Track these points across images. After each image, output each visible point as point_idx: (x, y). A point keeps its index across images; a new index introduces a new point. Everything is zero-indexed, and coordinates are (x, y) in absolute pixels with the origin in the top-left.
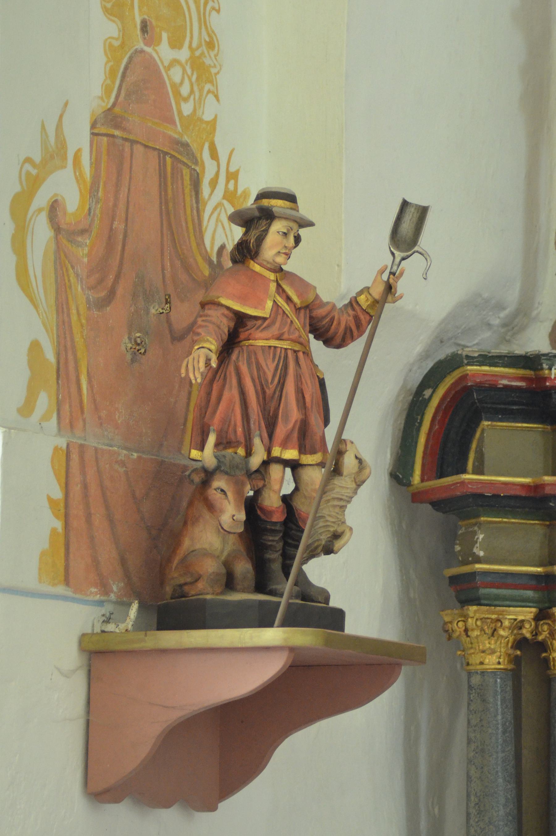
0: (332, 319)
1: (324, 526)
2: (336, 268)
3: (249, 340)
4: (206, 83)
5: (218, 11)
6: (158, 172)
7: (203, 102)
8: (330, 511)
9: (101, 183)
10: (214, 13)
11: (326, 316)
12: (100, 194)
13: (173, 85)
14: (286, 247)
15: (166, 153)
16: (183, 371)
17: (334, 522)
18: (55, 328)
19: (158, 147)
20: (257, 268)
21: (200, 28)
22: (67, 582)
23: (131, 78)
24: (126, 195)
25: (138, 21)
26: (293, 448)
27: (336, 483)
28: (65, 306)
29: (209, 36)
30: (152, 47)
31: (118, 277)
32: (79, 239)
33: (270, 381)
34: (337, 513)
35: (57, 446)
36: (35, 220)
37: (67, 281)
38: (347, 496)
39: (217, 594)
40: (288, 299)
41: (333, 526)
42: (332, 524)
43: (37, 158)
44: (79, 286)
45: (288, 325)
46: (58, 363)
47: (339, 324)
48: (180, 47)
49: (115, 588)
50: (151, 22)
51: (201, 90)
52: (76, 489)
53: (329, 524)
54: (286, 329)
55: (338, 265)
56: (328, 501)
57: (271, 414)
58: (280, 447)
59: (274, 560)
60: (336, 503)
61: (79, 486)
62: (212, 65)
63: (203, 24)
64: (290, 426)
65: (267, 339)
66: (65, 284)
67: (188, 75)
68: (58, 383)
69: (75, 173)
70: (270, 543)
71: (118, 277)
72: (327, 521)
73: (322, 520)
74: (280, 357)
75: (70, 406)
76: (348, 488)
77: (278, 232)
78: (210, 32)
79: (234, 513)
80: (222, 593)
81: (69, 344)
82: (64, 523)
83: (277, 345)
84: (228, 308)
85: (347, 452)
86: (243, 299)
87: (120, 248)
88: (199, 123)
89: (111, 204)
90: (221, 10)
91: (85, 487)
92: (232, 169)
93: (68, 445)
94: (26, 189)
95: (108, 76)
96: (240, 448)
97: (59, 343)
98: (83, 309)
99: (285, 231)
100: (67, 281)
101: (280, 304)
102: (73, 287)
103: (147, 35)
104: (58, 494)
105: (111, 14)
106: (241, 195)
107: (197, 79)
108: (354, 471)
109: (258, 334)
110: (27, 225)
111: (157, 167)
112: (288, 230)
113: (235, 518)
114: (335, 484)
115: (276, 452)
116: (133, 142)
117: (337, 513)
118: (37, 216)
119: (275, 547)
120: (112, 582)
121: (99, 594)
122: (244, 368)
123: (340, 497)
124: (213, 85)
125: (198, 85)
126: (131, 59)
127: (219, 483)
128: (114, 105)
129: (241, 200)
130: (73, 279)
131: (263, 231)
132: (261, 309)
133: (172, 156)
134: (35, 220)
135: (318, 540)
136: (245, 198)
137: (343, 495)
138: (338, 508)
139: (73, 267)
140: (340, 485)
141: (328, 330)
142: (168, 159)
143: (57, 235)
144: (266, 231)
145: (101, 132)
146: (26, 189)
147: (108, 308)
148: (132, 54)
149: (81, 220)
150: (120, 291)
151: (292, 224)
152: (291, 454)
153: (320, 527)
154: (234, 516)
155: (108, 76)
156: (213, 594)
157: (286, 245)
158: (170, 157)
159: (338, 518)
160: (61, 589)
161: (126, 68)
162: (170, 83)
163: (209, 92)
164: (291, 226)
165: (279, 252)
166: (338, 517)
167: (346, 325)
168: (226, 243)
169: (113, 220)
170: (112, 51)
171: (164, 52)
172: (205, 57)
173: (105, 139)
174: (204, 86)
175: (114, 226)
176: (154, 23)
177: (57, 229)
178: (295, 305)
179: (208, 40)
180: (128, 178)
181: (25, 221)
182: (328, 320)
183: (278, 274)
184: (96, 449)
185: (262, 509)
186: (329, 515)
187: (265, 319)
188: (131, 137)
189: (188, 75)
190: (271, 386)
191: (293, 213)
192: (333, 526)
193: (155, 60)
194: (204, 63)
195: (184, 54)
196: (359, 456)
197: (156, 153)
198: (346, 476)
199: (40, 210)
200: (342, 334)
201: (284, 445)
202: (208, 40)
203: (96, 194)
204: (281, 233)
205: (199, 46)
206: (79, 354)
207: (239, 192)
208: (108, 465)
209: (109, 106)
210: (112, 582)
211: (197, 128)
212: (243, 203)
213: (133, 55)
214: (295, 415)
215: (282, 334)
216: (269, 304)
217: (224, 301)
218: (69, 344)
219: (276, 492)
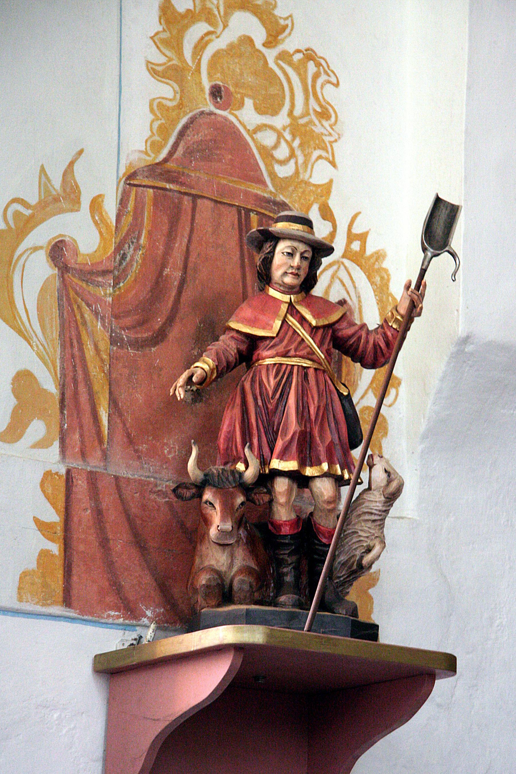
0: (360, 338)
1: (357, 542)
2: (456, 312)
3: (259, 360)
4: (315, 149)
5: (337, 85)
6: (236, 226)
7: (310, 167)
8: (362, 526)
9: (144, 232)
10: (329, 88)
11: (353, 335)
12: (142, 241)
13: (262, 149)
14: (292, 267)
15: (248, 211)
16: (172, 391)
17: (367, 537)
18: (58, 361)
19: (237, 204)
20: (272, 292)
21: (307, 99)
22: (67, 601)
23: (192, 137)
24: (184, 244)
25: (207, 85)
26: (293, 459)
27: (365, 497)
28: (75, 342)
29: (321, 106)
30: (229, 110)
31: (170, 320)
32: (100, 279)
33: (270, 396)
34: (369, 528)
35: (51, 471)
36: (28, 256)
37: (78, 317)
38: (376, 510)
39: (213, 607)
40: (302, 320)
41: (366, 541)
42: (366, 539)
43: (33, 199)
44: (99, 324)
45: (296, 343)
46: (63, 394)
47: (367, 341)
48: (275, 112)
49: (149, 613)
50: (227, 89)
51: (307, 156)
52: (84, 514)
53: (362, 539)
54: (293, 347)
55: (457, 310)
56: (359, 516)
57: (275, 429)
58: (277, 459)
59: (287, 574)
60: (367, 517)
61: (89, 511)
62: (325, 132)
63: (311, 94)
64: (289, 437)
65: (272, 357)
66: (76, 321)
67: (286, 141)
68: (62, 413)
69: (93, 217)
70: (281, 557)
71: (170, 320)
72: (360, 536)
73: (355, 535)
74: (284, 373)
75: (81, 436)
76: (376, 502)
77: (283, 253)
78: (323, 103)
79: (218, 524)
80: (219, 605)
81: (80, 377)
82: (62, 546)
83: (282, 362)
84: (238, 331)
85: (375, 466)
86: (253, 322)
87: (174, 293)
88: (304, 185)
89: (160, 252)
90: (341, 83)
91: (99, 514)
92: (357, 230)
93: (68, 472)
94: (13, 226)
95: (155, 131)
96: (239, 463)
97: (64, 375)
98: (104, 344)
99: (289, 251)
100: (78, 317)
101: (290, 323)
102: (89, 324)
103: (221, 99)
104: (52, 516)
105: (163, 77)
106: (372, 256)
107: (301, 145)
108: (383, 485)
109: (266, 353)
110: (14, 261)
111: (236, 222)
112: (293, 251)
113: (219, 528)
114: (364, 499)
115: (276, 464)
116: (195, 197)
117: (369, 528)
118: (31, 253)
119: (287, 561)
120: (143, 608)
121: (123, 617)
122: (247, 386)
123: (370, 511)
124: (327, 152)
125: (303, 151)
126: (192, 120)
127: (208, 495)
128: (166, 160)
129: (372, 260)
130: (88, 315)
131: (268, 253)
132: (269, 329)
133: (258, 213)
134: (28, 256)
135: (353, 556)
136: (377, 260)
137: (372, 509)
138: (370, 522)
139: (89, 305)
140: (368, 499)
141: (357, 349)
142: (252, 215)
143: (62, 273)
144: (273, 252)
145: (144, 184)
146: (13, 226)
147: (153, 349)
148: (195, 115)
149: (103, 261)
150: (174, 333)
151: (296, 244)
152: (291, 465)
153: (354, 543)
154: (218, 526)
155: (155, 131)
156: (208, 606)
157: (292, 265)
158: (256, 214)
159: (370, 533)
160: (58, 610)
161: (186, 127)
162: (256, 146)
163: (320, 157)
164: (295, 246)
165: (286, 272)
166: (371, 531)
167: (374, 343)
168: (348, 299)
169: (163, 266)
170: (157, 107)
171: (247, 116)
172: (315, 125)
173: (151, 191)
174: (312, 152)
175: (165, 273)
176: (232, 89)
177: (64, 269)
178: (310, 324)
179: (319, 109)
180: (188, 229)
181: (12, 256)
182: (355, 339)
183: (292, 296)
184: (117, 478)
185: (272, 524)
186: (361, 530)
187: (273, 338)
188: (193, 192)
189: (286, 141)
190: (272, 401)
191: (310, 236)
192: (366, 541)
193: (231, 123)
194: (312, 131)
195: (281, 120)
196: (388, 469)
197: (234, 210)
198: (374, 490)
199: (36, 249)
200: (372, 351)
201: (282, 457)
202: (319, 109)
203: (135, 241)
204: (285, 254)
205: (306, 114)
206: (96, 387)
207: (368, 252)
208: (138, 494)
209: (157, 161)
210: (143, 608)
211: (300, 190)
212: (374, 264)
213: (198, 116)
214: (293, 426)
215: (289, 351)
216: (278, 324)
217: (233, 325)
218: (80, 377)
219: (282, 505)
